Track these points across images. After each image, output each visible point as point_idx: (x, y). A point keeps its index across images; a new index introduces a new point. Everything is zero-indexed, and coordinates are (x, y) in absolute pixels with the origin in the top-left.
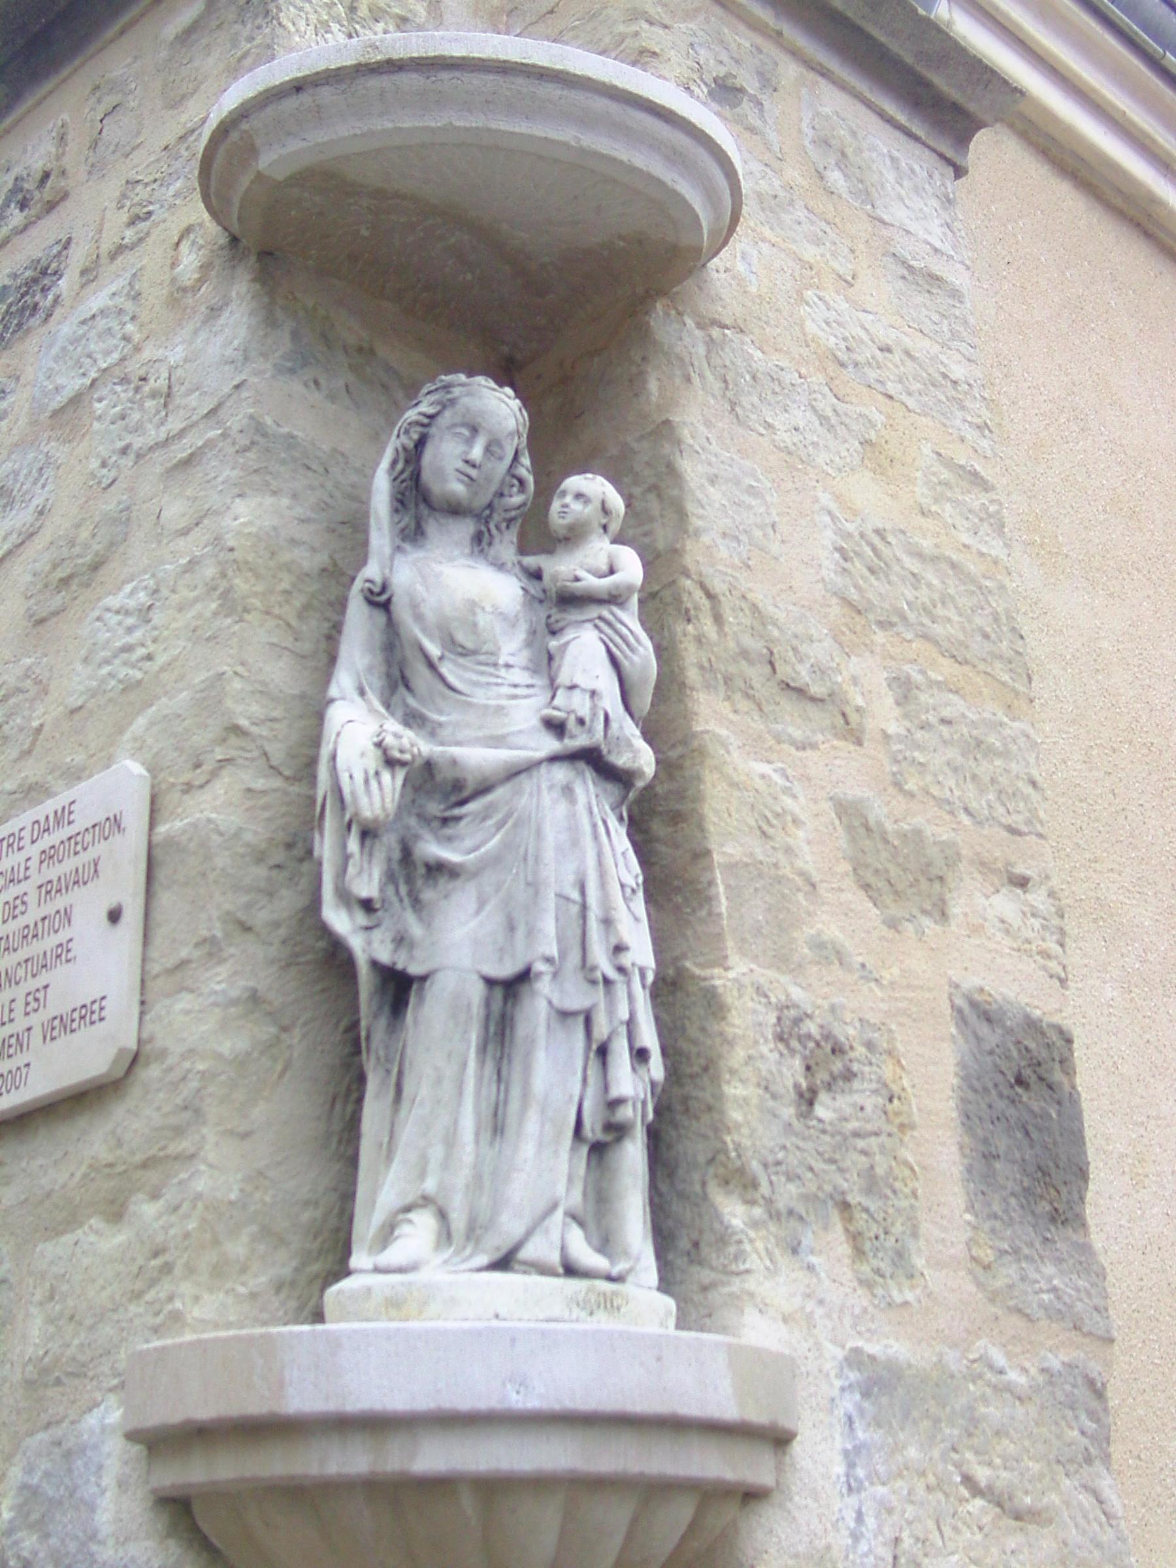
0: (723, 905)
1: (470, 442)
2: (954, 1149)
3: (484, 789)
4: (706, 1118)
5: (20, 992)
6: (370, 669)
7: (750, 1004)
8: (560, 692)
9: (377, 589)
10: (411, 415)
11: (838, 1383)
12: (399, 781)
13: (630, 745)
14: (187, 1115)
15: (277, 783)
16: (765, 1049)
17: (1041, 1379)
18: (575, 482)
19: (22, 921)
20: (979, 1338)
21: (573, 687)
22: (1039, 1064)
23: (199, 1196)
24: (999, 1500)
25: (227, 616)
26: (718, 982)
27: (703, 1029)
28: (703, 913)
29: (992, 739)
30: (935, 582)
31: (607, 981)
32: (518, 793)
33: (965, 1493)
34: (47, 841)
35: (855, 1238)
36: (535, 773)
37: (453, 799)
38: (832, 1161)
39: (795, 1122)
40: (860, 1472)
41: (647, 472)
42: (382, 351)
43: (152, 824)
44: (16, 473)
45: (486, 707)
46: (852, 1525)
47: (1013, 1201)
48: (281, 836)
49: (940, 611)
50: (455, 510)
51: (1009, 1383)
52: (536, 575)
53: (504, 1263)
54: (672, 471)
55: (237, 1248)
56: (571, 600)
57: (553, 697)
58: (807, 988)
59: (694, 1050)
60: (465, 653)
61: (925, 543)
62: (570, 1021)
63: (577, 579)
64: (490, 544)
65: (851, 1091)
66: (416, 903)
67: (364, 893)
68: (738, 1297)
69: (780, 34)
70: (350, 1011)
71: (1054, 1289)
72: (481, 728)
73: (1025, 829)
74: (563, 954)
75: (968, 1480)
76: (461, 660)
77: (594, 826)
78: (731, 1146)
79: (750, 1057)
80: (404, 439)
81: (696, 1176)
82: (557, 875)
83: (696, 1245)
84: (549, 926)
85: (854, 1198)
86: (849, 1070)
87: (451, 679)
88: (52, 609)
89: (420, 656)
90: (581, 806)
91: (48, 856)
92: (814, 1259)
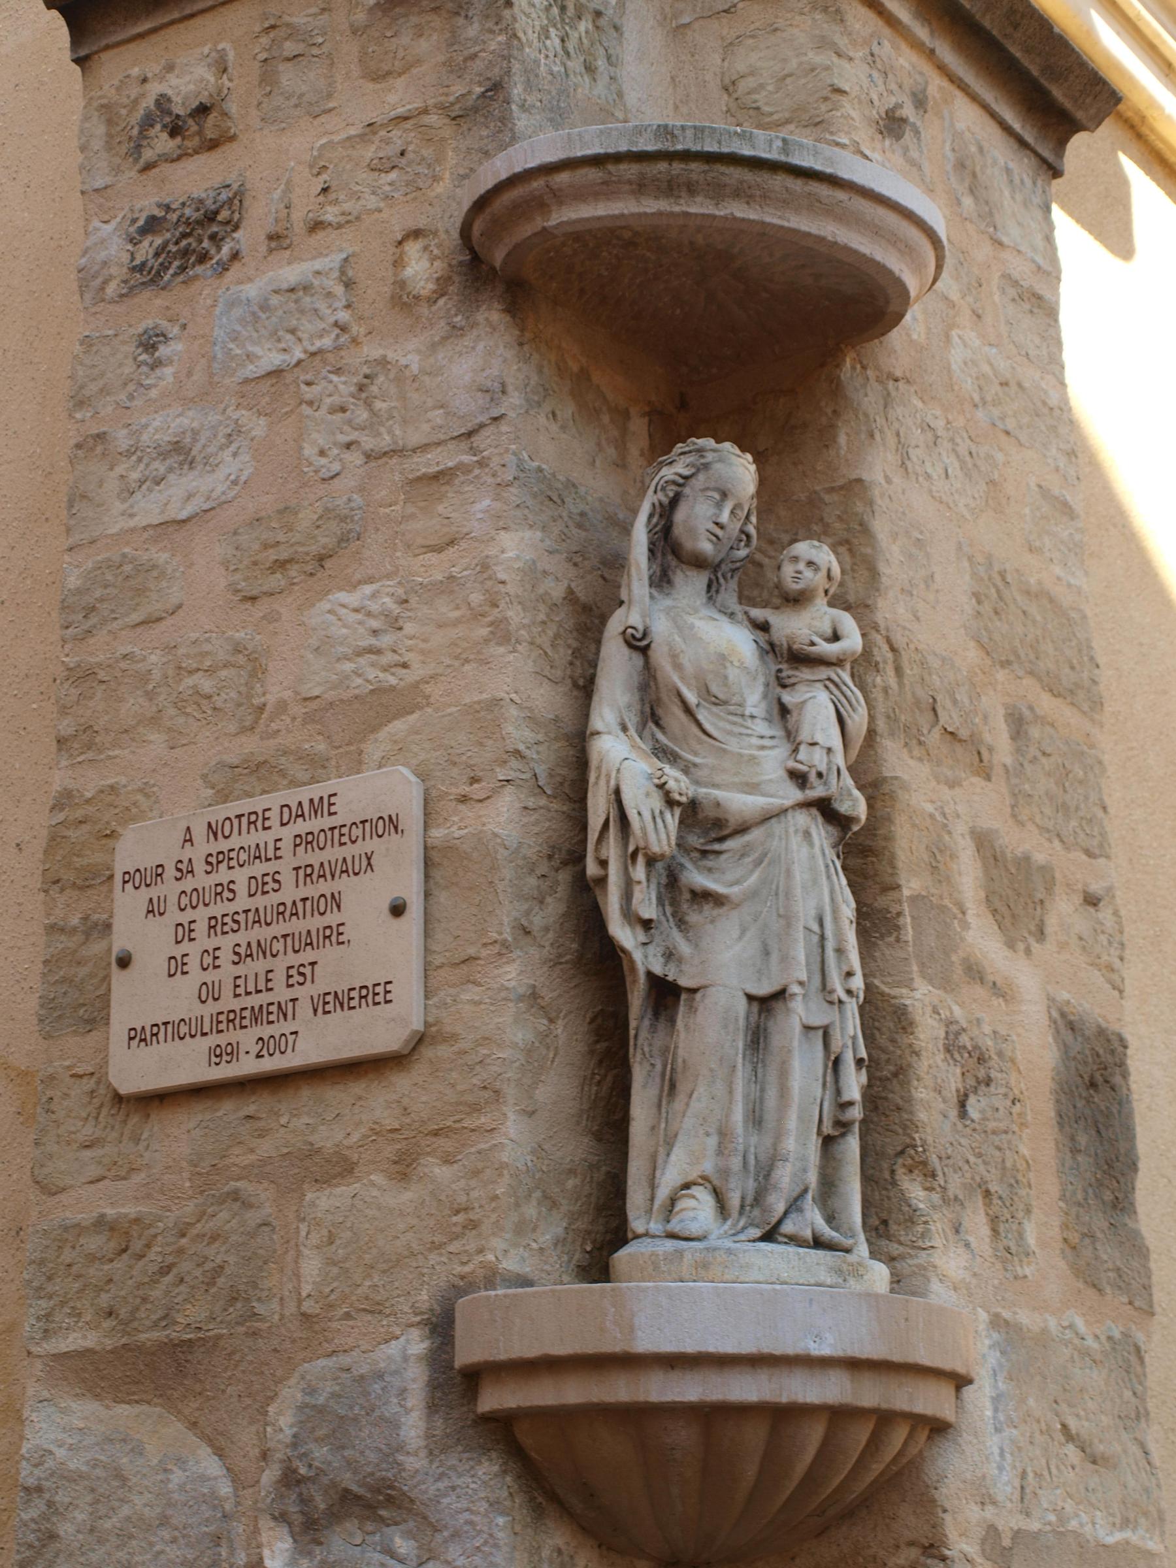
0: (909, 934)
1: (719, 505)
2: (1052, 1145)
3: (742, 830)
5: (280, 965)
6: (629, 706)
8: (802, 748)
9: (638, 636)
10: (668, 473)
11: (987, 1342)
13: (850, 794)
14: (486, 1094)
15: (543, 801)
17: (1108, 1346)
18: (803, 548)
19: (274, 898)
21: (813, 744)
22: (1105, 1069)
23: (503, 1166)
25: (499, 644)
26: (908, 1002)
27: (893, 1041)
28: (892, 939)
30: (1039, 618)
31: (840, 1002)
32: (770, 835)
33: (1063, 1439)
34: (301, 827)
36: (782, 818)
41: (837, 525)
42: (597, 377)
44: (195, 433)
45: (741, 755)
48: (546, 851)
50: (698, 562)
52: (763, 627)
53: (769, 1236)
54: (865, 530)
55: (531, 1211)
56: (800, 659)
57: (796, 750)
58: (962, 1005)
59: (884, 1057)
60: (718, 702)
62: (812, 1033)
63: (813, 644)
64: (717, 592)
66: (681, 923)
67: (646, 916)
68: (925, 1269)
69: (932, 51)
70: (614, 1011)
72: (736, 774)
73: (1097, 851)
77: (827, 866)
78: (919, 1143)
81: (885, 1165)
82: (804, 911)
83: (885, 1222)
85: (993, 1187)
87: (707, 726)
88: (265, 588)
89: (676, 700)
91: (304, 841)
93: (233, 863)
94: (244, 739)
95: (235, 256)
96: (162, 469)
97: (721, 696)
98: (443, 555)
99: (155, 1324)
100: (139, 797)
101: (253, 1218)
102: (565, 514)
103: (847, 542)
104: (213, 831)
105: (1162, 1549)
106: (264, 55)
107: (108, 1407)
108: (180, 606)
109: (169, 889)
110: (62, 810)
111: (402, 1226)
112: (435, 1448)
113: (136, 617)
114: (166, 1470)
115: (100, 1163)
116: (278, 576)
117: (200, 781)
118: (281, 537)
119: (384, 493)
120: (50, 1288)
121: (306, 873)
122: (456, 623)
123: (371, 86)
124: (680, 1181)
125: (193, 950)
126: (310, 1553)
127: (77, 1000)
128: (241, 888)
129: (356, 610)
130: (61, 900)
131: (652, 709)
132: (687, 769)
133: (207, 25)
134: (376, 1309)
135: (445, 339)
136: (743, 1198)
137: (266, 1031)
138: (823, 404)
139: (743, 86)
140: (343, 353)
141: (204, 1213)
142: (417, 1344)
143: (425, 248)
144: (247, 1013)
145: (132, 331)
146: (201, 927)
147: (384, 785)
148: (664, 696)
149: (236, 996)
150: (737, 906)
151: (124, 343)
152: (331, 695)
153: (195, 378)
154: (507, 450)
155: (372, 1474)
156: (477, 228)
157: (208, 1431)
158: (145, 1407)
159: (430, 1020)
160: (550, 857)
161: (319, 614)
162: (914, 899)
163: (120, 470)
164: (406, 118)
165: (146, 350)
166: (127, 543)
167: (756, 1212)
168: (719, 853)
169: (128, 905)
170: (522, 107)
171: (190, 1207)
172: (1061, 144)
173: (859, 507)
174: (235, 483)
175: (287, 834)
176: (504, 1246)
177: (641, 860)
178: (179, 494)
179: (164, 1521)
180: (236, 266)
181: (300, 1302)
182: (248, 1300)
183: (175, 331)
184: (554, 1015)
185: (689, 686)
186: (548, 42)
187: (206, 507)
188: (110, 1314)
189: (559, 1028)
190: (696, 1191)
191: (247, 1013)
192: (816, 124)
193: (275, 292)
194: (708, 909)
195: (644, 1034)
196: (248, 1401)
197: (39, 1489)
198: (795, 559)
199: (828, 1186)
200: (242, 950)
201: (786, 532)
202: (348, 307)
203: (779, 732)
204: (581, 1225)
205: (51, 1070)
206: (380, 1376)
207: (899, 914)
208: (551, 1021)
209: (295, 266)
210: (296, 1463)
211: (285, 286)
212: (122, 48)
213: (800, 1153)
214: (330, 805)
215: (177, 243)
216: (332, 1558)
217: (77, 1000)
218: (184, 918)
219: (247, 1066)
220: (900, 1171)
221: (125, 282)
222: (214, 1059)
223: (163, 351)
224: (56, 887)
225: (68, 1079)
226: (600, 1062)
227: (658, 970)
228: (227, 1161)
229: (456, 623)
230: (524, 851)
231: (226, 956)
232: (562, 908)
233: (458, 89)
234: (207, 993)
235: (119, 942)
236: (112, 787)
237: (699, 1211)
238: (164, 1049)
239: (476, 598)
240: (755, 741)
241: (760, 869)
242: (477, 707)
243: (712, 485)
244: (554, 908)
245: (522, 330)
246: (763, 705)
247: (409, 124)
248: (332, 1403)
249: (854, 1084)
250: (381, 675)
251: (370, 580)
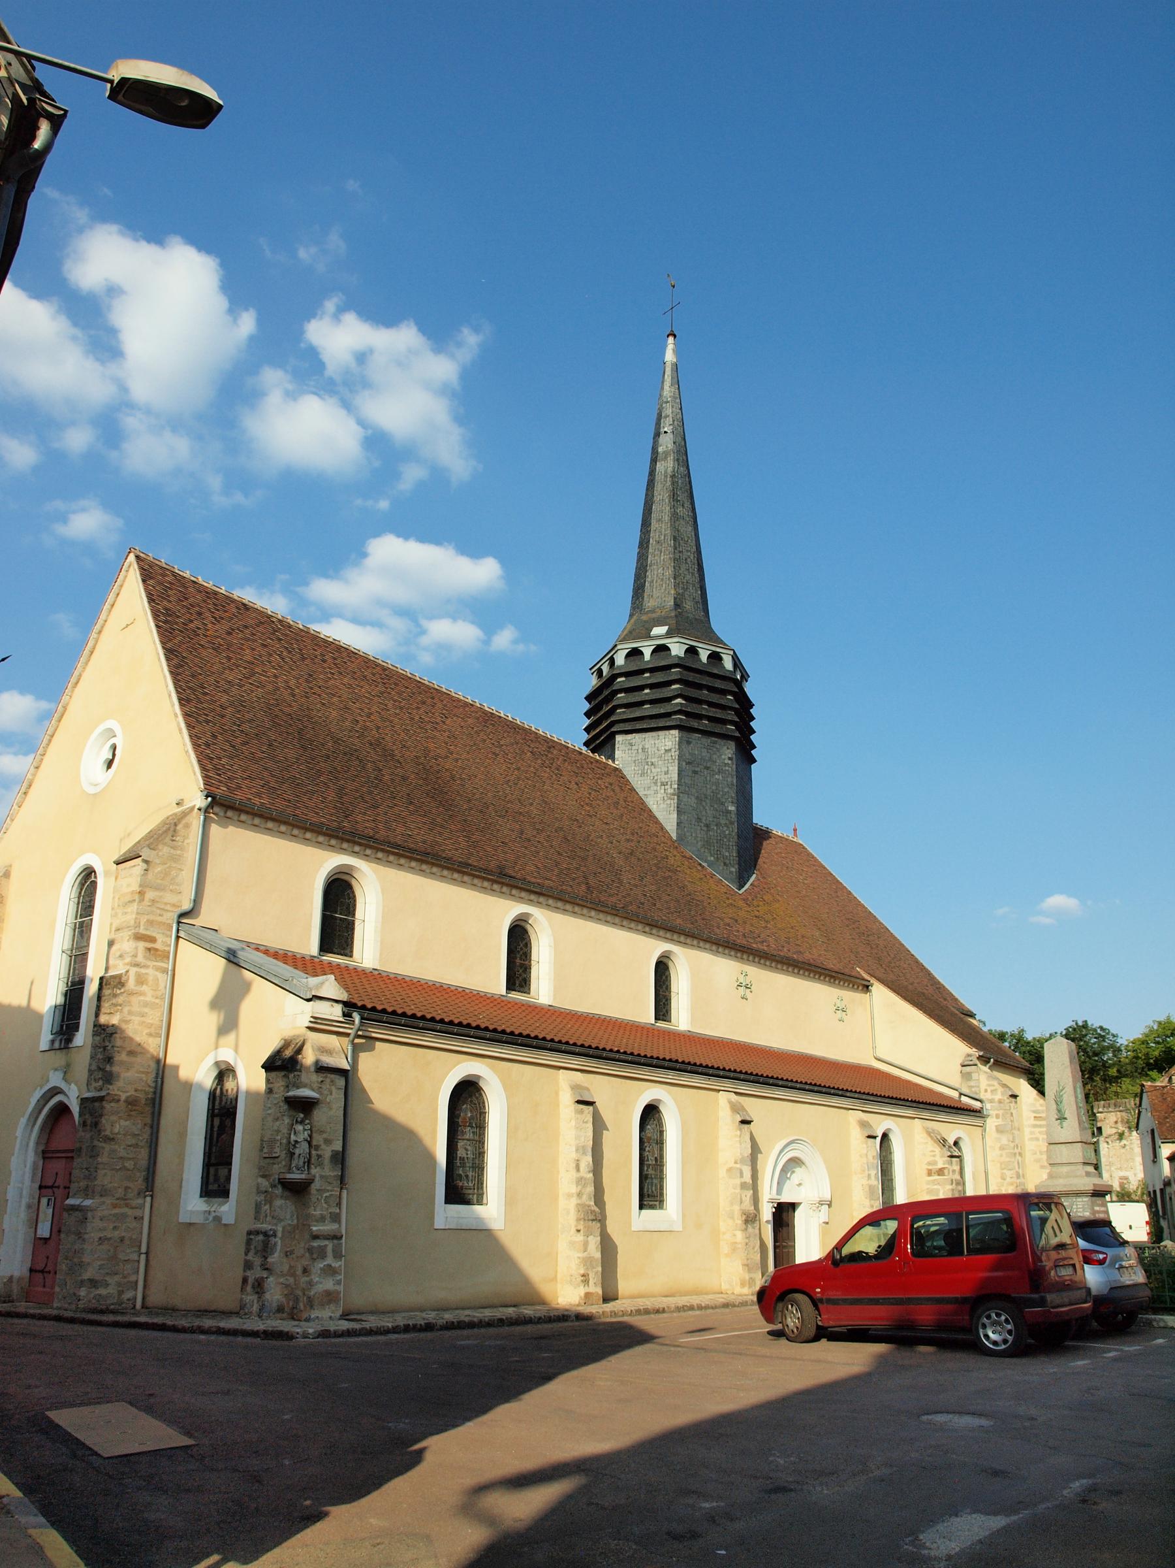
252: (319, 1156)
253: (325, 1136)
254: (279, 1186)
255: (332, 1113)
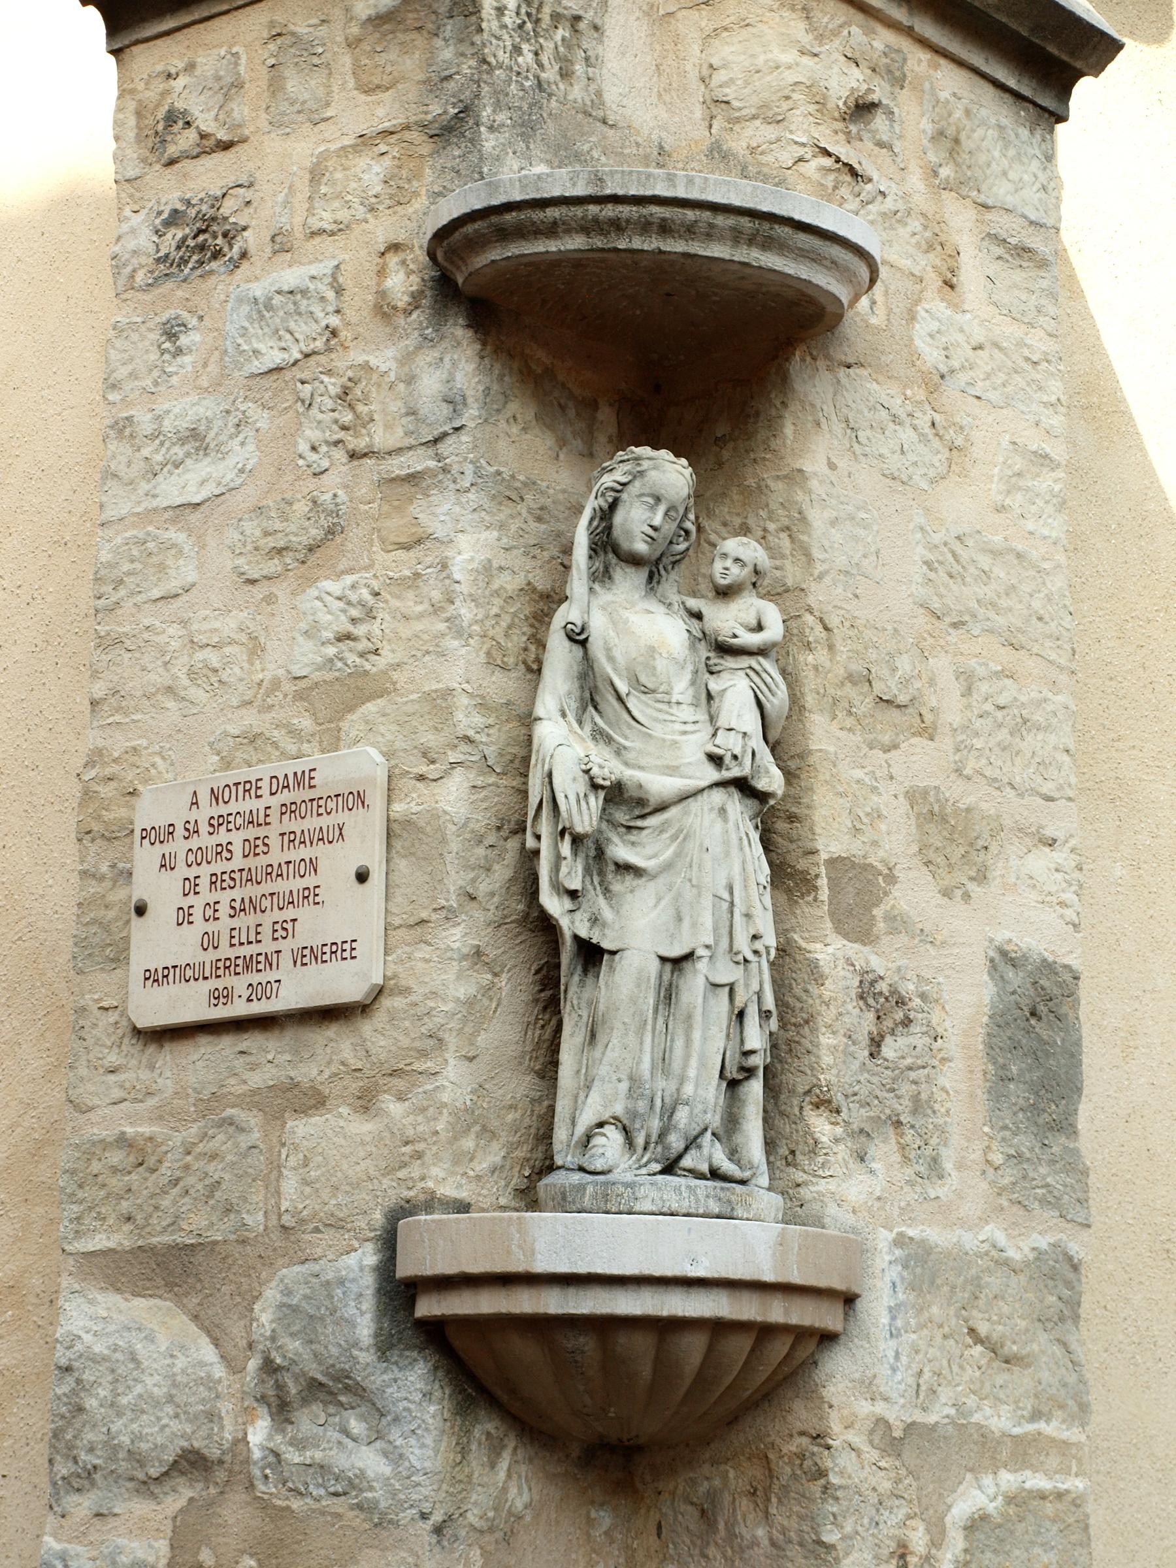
0: (824, 894)
1: (653, 508)
3: (662, 808)
4: (806, 1060)
5: (267, 920)
7: (842, 973)
8: (719, 733)
10: (608, 480)
11: (887, 1258)
12: (601, 802)
13: (767, 772)
14: (431, 1042)
15: (492, 779)
16: (850, 1007)
19: (263, 860)
20: (987, 1223)
24: (993, 1349)
25: (454, 638)
27: (806, 991)
28: (810, 898)
29: (1038, 717)
31: (746, 961)
32: (686, 813)
33: (969, 1341)
34: (285, 797)
35: (903, 1148)
37: (637, 812)
38: (893, 1090)
39: (867, 1062)
40: (899, 1323)
43: (389, 801)
45: (664, 740)
46: (892, 1361)
47: (1021, 1115)
48: (495, 822)
49: (1004, 603)
50: (635, 560)
51: (1007, 1259)
53: (670, 1168)
56: (725, 649)
57: (714, 735)
59: (798, 1005)
60: (647, 691)
61: (996, 538)
63: (735, 636)
65: (908, 1034)
67: (573, 887)
69: (911, 28)
70: (554, 964)
71: (1047, 1185)
73: (1056, 795)
74: (717, 942)
75: (972, 1331)
76: (643, 697)
79: (840, 1014)
80: (601, 501)
83: (793, 1152)
84: (707, 920)
86: (907, 1018)
87: (635, 713)
88: (265, 573)
90: (731, 825)
91: (289, 809)
92: (874, 1165)
93: (231, 826)
94: (244, 711)
95: (244, 255)
96: (181, 454)
97: (649, 685)
98: (412, 554)
99: (165, 1229)
100: (158, 760)
101: (244, 1141)
102: (524, 511)
103: (788, 528)
104: (215, 796)
105: (1083, 1438)
106: (272, 61)
107: (126, 1300)
108: (193, 585)
109: (178, 846)
110: (94, 767)
111: (362, 1154)
112: (385, 1347)
113: (156, 593)
114: (172, 1356)
115: (121, 1087)
116: (276, 561)
117: (207, 748)
118: (278, 525)
119: (364, 491)
120: (80, 1194)
121: (291, 839)
122: (420, 616)
123: (363, 97)
124: (595, 1121)
125: (198, 902)
126: (283, 1431)
127: (104, 941)
128: (237, 849)
129: (339, 599)
130: (93, 848)
131: (592, 693)
132: (619, 751)
133: (223, 28)
134: (338, 1225)
135: (419, 348)
136: (648, 1136)
137: (255, 978)
138: (773, 396)
139: (719, 77)
140: (333, 356)
141: (206, 1134)
142: (368, 1256)
143: (403, 262)
144: (240, 962)
145: (158, 320)
146: (204, 882)
147: (361, 761)
148: (600, 684)
149: (232, 945)
150: (654, 877)
151: (150, 330)
152: (317, 676)
153: (209, 369)
154: (465, 459)
155: (333, 1366)
156: (440, 255)
157: (207, 1323)
158: (157, 1301)
159: (389, 974)
160: (499, 828)
161: (308, 600)
162: (832, 862)
163: (146, 452)
164: (392, 133)
165: (169, 339)
166: (151, 522)
167: (659, 1149)
168: (641, 829)
169: (146, 857)
170: (491, 128)
171: (194, 1129)
172: (1064, 91)
173: (800, 496)
174: (242, 471)
175: (275, 802)
176: (442, 1175)
177: (567, 837)
178: (192, 481)
179: (170, 1399)
180: (245, 265)
181: (280, 1216)
182: (238, 1212)
183: (193, 322)
184: (498, 969)
185: (620, 675)
186: (520, 59)
187: (217, 492)
188: (129, 1219)
189: (503, 981)
190: (608, 1129)
191: (240, 962)
192: (779, 122)
193: (279, 292)
194: (629, 879)
195: (573, 989)
196: (238, 1299)
197: (68, 1369)
198: (725, 556)
199: (732, 1121)
200: (237, 905)
201: (738, 514)
202: (338, 312)
203: (702, 716)
204: (521, 1153)
205: (82, 1002)
206: (341, 1282)
207: (817, 876)
208: (496, 975)
209: (294, 268)
210: (274, 1354)
211: (286, 288)
212: (152, 43)
213: (704, 1095)
214: (311, 778)
215: (195, 237)
216: (300, 1435)
217: (104, 941)
218: (191, 873)
219: (240, 1008)
220: (808, 1108)
221: (151, 272)
222: (213, 1001)
223: (183, 340)
224: (88, 837)
225: (96, 1011)
226: (545, 1008)
227: (583, 933)
228: (225, 1090)
229: (420, 616)
230: (471, 825)
231: (224, 910)
232: (509, 873)
233: (436, 109)
234: (209, 942)
235: (139, 892)
236: (135, 749)
237: (610, 1143)
238: (172, 989)
239: (436, 595)
240: (679, 727)
241: (676, 844)
242: (434, 695)
243: (647, 491)
244: (503, 872)
245: (484, 344)
246: (691, 692)
247: (393, 139)
248: (304, 1304)
249: (755, 1038)
250: (358, 660)
251: (351, 571)
252: (887, 1007)
253: (921, 762)
254: (414, 1390)
255: (963, 506)
